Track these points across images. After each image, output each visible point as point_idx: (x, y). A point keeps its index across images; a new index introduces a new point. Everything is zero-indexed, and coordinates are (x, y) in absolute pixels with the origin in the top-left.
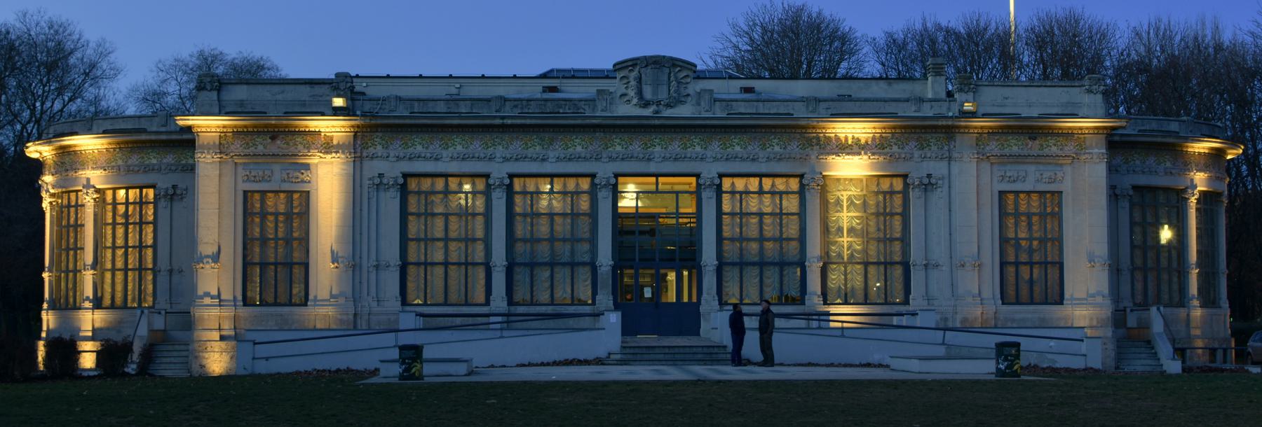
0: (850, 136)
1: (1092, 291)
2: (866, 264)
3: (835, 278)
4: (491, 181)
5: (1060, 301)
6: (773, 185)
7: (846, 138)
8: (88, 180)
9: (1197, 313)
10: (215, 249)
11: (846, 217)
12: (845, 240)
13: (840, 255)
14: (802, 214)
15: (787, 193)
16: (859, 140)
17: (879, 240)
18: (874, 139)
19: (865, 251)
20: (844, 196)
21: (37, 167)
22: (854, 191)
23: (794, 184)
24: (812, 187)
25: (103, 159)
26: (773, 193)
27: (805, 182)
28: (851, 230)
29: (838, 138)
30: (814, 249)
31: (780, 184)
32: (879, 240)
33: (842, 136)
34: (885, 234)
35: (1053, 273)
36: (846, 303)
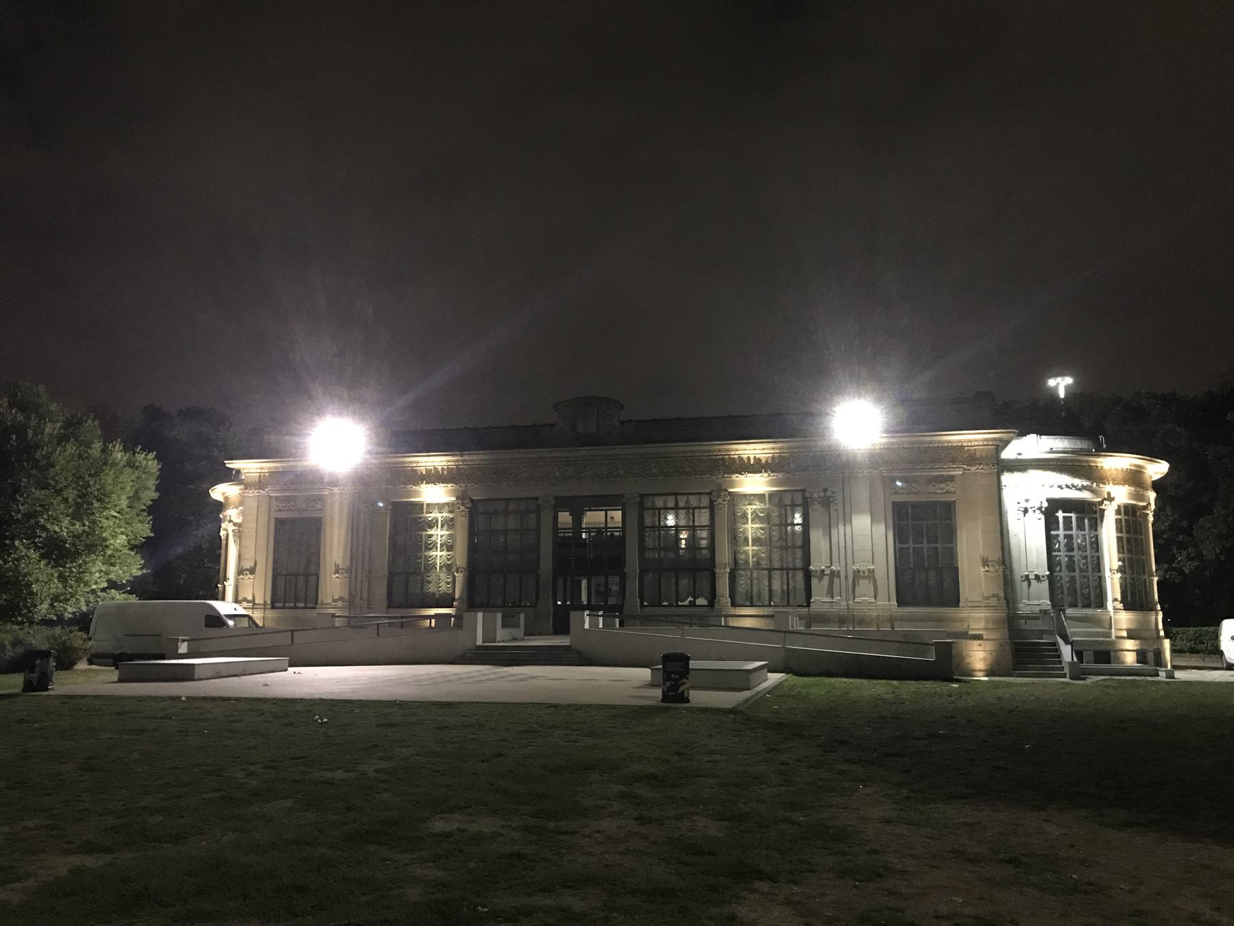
0: (752, 457)
1: (336, 597)
2: (770, 570)
3: (743, 583)
4: (539, 502)
5: (955, 602)
6: (687, 502)
7: (749, 459)
8: (1109, 494)
9: (1123, 619)
10: (252, 564)
11: (751, 528)
12: (750, 549)
13: (747, 562)
14: (712, 528)
15: (700, 508)
16: (760, 460)
17: (781, 548)
18: (773, 458)
19: (770, 558)
20: (749, 509)
21: (220, 507)
22: (757, 506)
23: (705, 501)
24: (720, 503)
25: (1120, 476)
26: (686, 508)
27: (807, 495)
28: (756, 541)
29: (741, 459)
30: (724, 556)
31: (694, 501)
32: (781, 548)
33: (745, 457)
34: (786, 542)
35: (312, 579)
36: (752, 605)
